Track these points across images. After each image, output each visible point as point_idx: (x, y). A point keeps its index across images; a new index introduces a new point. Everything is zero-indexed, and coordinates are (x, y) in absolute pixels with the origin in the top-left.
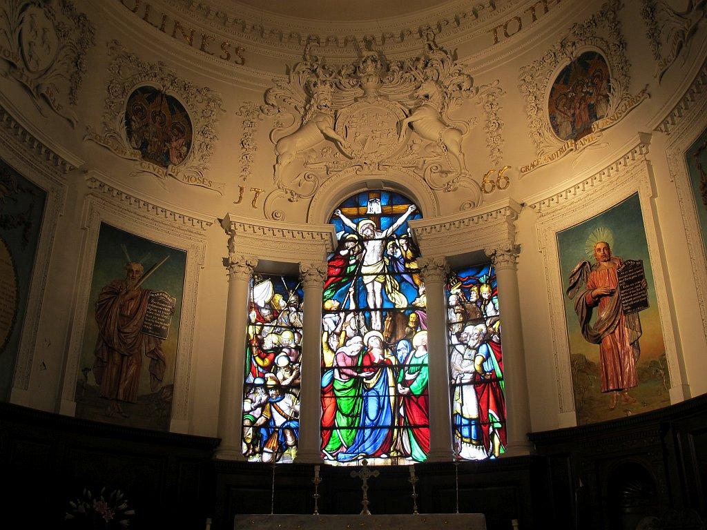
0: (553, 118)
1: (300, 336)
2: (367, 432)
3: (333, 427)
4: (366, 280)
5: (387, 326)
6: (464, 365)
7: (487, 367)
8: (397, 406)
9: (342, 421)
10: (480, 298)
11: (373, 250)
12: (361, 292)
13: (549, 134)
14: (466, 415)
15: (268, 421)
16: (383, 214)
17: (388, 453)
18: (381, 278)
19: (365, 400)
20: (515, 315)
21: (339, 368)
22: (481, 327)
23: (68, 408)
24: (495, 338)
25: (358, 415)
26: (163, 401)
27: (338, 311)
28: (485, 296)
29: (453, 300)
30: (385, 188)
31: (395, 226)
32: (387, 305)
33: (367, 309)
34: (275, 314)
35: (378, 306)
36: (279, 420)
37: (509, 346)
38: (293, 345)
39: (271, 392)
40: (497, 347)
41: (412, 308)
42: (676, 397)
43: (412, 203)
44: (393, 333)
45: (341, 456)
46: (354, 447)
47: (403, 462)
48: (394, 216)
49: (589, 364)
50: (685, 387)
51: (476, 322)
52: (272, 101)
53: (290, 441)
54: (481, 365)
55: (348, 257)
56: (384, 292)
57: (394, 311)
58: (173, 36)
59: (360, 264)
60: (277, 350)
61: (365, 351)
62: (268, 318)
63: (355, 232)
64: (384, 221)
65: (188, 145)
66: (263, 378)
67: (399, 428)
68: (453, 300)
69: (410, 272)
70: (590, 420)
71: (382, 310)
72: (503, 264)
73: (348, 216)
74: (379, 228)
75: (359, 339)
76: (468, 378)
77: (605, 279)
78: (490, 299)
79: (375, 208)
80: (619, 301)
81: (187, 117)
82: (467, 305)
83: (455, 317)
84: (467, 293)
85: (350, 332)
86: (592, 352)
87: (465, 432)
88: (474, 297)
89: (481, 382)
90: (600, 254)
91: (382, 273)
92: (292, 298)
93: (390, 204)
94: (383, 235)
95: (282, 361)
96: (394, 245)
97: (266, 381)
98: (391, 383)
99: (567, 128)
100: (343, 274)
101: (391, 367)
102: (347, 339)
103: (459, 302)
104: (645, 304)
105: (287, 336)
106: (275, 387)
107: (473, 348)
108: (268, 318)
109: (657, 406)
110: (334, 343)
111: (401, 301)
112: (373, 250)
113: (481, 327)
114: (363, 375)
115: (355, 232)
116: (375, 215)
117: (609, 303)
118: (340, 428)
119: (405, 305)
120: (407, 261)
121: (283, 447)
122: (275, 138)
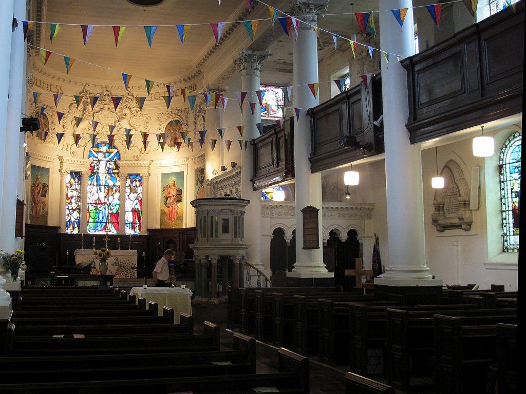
2: (99, 224)
3: (88, 222)
4: (100, 175)
5: (106, 191)
6: (130, 205)
8: (108, 216)
9: (91, 220)
12: (98, 179)
15: (70, 220)
17: (105, 230)
18: (105, 175)
19: (99, 213)
20: (147, 192)
22: (135, 195)
24: (140, 199)
26: (45, 216)
29: (127, 185)
32: (106, 184)
34: (71, 185)
37: (144, 202)
40: (141, 201)
41: (115, 186)
42: (184, 227)
44: (108, 193)
45: (91, 231)
46: (95, 228)
47: (109, 233)
48: (110, 153)
49: (165, 213)
50: (186, 224)
51: (134, 193)
56: (105, 180)
57: (109, 186)
59: (98, 169)
60: (72, 197)
61: (99, 199)
63: (97, 158)
64: (107, 154)
67: (109, 223)
68: (127, 185)
69: (114, 173)
70: (164, 227)
71: (105, 185)
73: (94, 151)
74: (105, 157)
81: (47, 119)
82: (132, 187)
83: (128, 190)
84: (132, 183)
85: (95, 193)
86: (167, 210)
87: (128, 225)
88: (134, 185)
89: (135, 212)
92: (76, 180)
93: (109, 148)
98: (107, 209)
100: (93, 172)
104: (181, 201)
109: (180, 227)
111: (111, 183)
114: (98, 206)
115: (97, 158)
117: (173, 198)
120: (113, 169)
121: (74, 228)
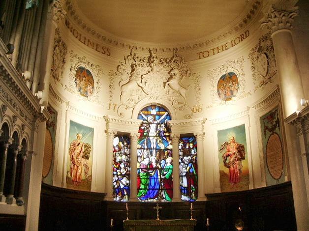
0: (218, 91)
1: (128, 157)
4: (151, 138)
7: (191, 171)
10: (189, 148)
11: (153, 127)
13: (217, 97)
14: (183, 186)
16: (157, 115)
21: (141, 169)
23: (65, 187)
24: (194, 161)
25: (148, 185)
27: (141, 149)
28: (191, 147)
30: (157, 105)
31: (161, 119)
32: (158, 148)
33: (151, 149)
34: (120, 149)
35: (155, 148)
36: (122, 186)
38: (126, 160)
39: (119, 177)
43: (166, 111)
44: (160, 157)
48: (160, 116)
52: (120, 70)
53: (125, 193)
54: (189, 170)
55: (144, 129)
56: (157, 144)
57: (160, 150)
58: (88, 46)
59: (148, 132)
60: (121, 162)
61: (150, 164)
62: (118, 150)
63: (147, 120)
65: (93, 88)
66: (116, 171)
67: (161, 190)
69: (165, 136)
72: (200, 139)
73: (144, 114)
74: (155, 120)
75: (148, 159)
76: (184, 174)
77: (233, 149)
78: (193, 148)
79: (154, 112)
80: (236, 157)
84: (185, 145)
88: (187, 147)
90: (231, 141)
91: (156, 136)
92: (125, 144)
93: (159, 111)
94: (156, 122)
95: (122, 166)
96: (160, 126)
97: (117, 173)
98: (159, 174)
99: (223, 96)
101: (159, 169)
102: (144, 159)
103: (182, 148)
104: (244, 159)
105: (124, 157)
106: (120, 175)
107: (186, 164)
108: (118, 150)
110: (139, 159)
112: (153, 127)
113: (189, 157)
114: (150, 171)
115: (147, 120)
116: (153, 115)
117: (233, 157)
118: (142, 189)
119: (164, 148)
120: (165, 132)
121: (123, 195)
122: (121, 85)
